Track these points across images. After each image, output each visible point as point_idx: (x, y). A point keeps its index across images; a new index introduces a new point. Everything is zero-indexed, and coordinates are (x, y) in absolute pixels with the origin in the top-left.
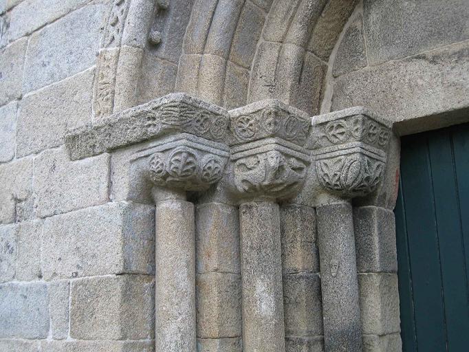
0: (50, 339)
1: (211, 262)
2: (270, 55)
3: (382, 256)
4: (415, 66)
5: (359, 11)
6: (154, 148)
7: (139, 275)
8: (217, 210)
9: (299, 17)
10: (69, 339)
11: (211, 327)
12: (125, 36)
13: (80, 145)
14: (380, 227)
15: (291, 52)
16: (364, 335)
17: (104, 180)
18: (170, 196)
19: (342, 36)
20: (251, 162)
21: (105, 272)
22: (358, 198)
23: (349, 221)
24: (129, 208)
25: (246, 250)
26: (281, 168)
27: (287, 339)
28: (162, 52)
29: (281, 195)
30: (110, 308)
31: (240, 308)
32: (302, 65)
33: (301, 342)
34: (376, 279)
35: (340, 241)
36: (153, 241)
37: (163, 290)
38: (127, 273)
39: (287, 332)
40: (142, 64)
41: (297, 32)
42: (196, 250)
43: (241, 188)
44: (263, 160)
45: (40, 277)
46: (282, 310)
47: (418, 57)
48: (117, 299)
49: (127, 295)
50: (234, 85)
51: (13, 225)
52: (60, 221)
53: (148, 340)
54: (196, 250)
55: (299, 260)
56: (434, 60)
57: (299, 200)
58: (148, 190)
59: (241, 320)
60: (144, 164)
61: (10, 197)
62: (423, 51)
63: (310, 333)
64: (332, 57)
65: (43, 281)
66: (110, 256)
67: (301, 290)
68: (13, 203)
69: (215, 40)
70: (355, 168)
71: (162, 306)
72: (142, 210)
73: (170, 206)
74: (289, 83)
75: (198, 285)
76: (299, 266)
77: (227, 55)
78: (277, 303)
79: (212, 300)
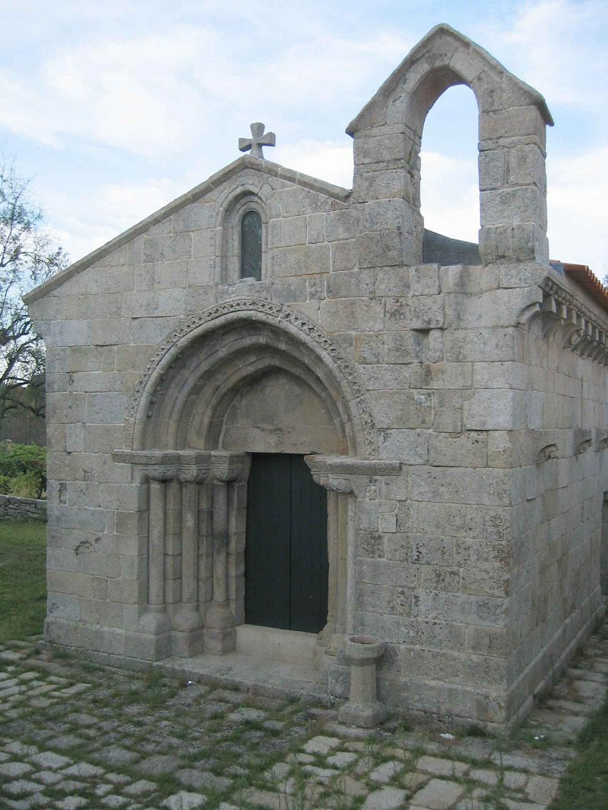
0: (106, 532)
1: (171, 506)
2: (198, 419)
3: (238, 503)
4: (256, 430)
5: (238, 397)
6: (151, 467)
7: (144, 511)
8: (174, 487)
9: (210, 407)
10: (115, 533)
11: (170, 530)
12: (138, 417)
13: (117, 457)
14: (238, 493)
15: (206, 420)
16: (174, 633)
17: (129, 474)
18: (156, 482)
19: (230, 407)
20: (187, 472)
21: (131, 510)
22: (229, 483)
23: (225, 491)
24: (141, 487)
25: (184, 502)
26: (198, 475)
27: (198, 534)
28: (152, 419)
29: (199, 482)
30: (133, 524)
31: (181, 522)
32: (211, 424)
33: (203, 535)
34: (234, 513)
35: (221, 498)
36: (148, 497)
37: (153, 517)
38: (140, 511)
39: (198, 532)
40: (146, 425)
41: (209, 413)
42: (165, 500)
43: (183, 480)
44: (191, 472)
45: (100, 507)
46: (196, 562)
47: (258, 427)
48: (136, 521)
49: (140, 519)
50: (182, 442)
51: (84, 482)
52: (109, 486)
53: (146, 535)
54: (165, 500)
55: (204, 505)
56: (263, 430)
57: (206, 482)
58: (147, 480)
59: (181, 528)
60: (147, 472)
61: (81, 470)
62: (259, 425)
63: (207, 532)
64: (226, 415)
65: (100, 509)
66: (133, 505)
67: (204, 516)
68: (83, 473)
69: (175, 417)
70: (226, 475)
71: (152, 523)
72: (145, 486)
73: (155, 487)
74: (205, 434)
75: (165, 514)
76: (204, 507)
77: (179, 421)
78: (195, 521)
79: (171, 520)
